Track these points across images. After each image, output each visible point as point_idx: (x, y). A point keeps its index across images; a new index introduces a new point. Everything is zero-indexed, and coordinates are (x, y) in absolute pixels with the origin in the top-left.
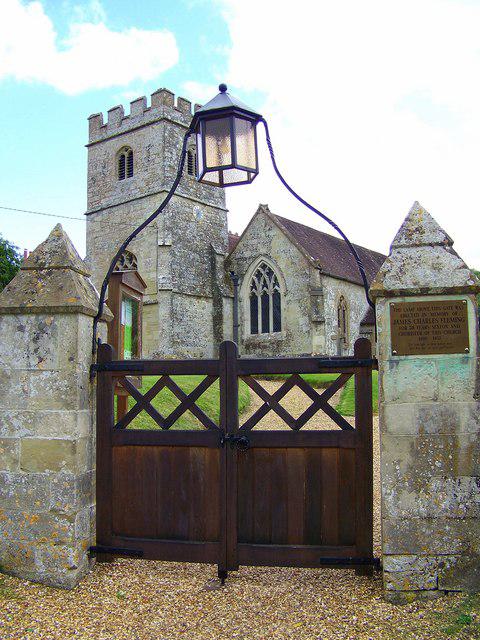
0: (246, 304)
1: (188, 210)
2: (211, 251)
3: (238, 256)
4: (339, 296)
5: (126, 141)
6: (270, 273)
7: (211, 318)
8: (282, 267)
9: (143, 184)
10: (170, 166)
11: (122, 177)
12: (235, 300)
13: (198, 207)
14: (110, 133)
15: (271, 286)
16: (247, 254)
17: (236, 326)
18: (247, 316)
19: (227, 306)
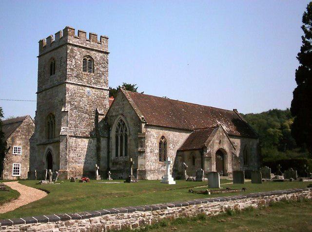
0: (113, 140)
1: (82, 91)
2: (97, 114)
3: (111, 115)
4: (160, 136)
5: (53, 54)
6: (124, 124)
7: (95, 148)
8: (128, 121)
9: (58, 78)
10: (70, 69)
11: (51, 74)
12: (109, 138)
13: (88, 89)
14: (47, 50)
15: (124, 132)
16: (114, 114)
17: (109, 152)
18: (114, 147)
19: (104, 143)
